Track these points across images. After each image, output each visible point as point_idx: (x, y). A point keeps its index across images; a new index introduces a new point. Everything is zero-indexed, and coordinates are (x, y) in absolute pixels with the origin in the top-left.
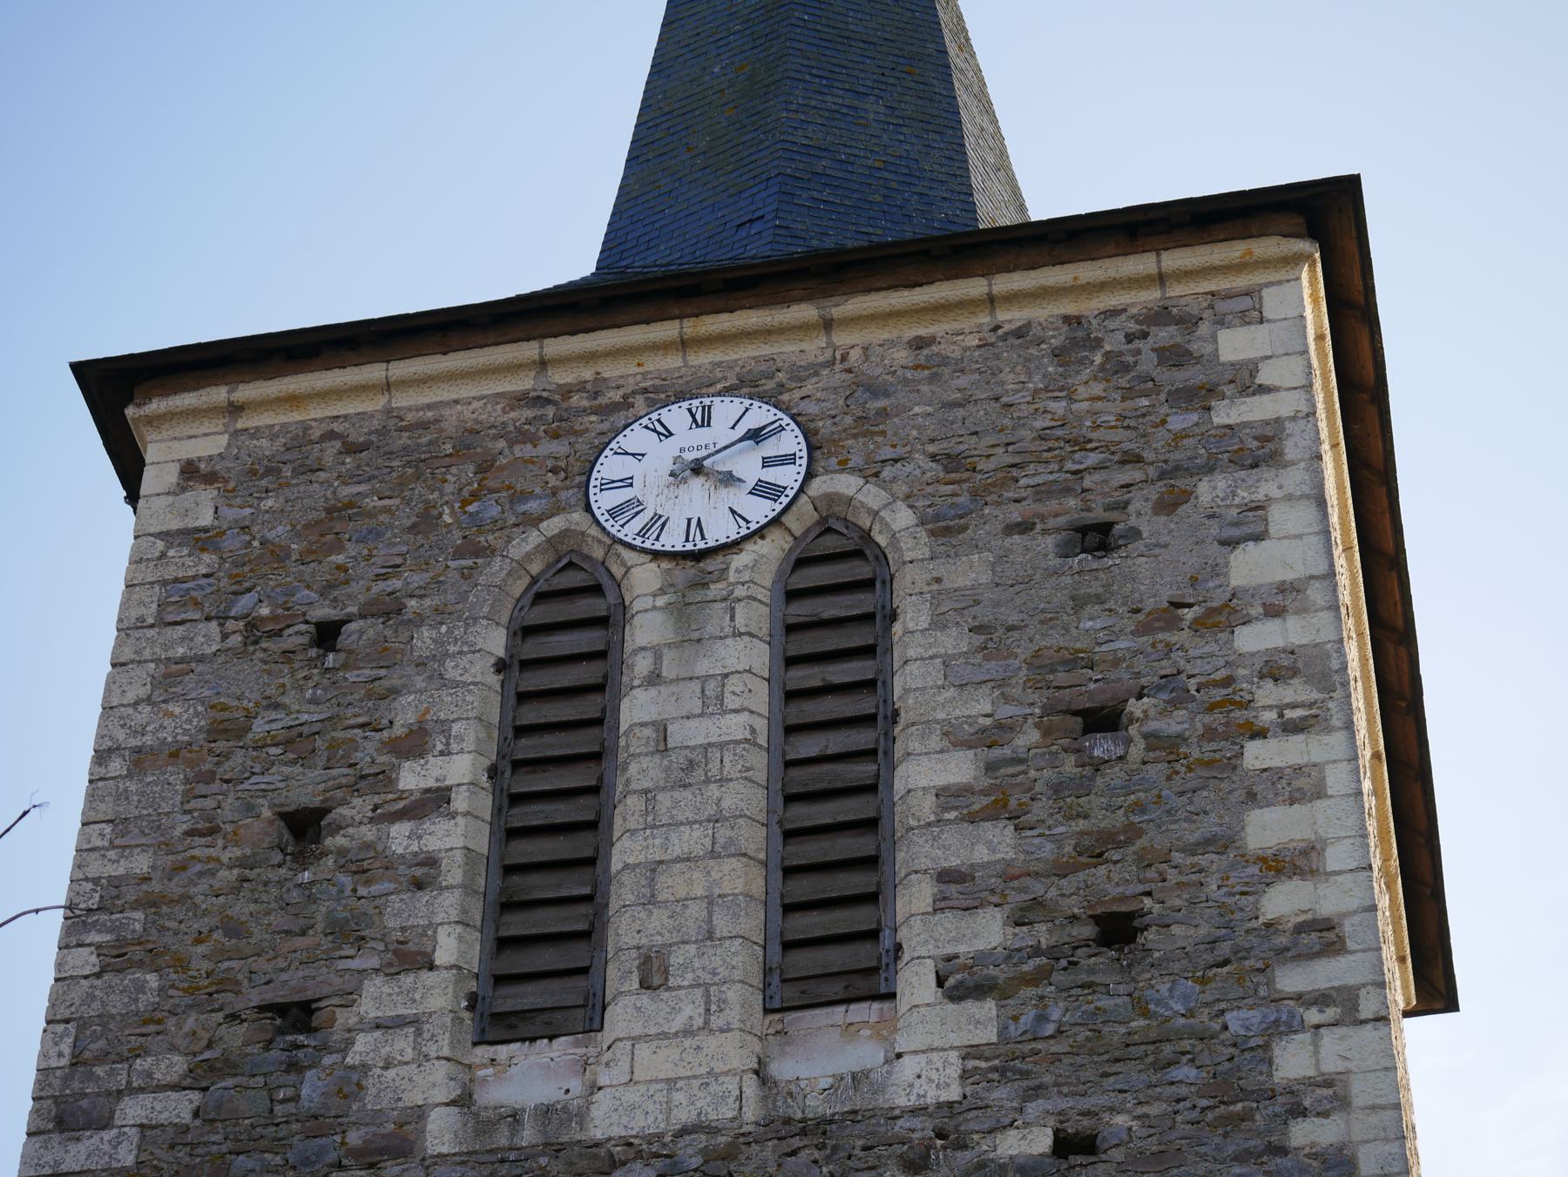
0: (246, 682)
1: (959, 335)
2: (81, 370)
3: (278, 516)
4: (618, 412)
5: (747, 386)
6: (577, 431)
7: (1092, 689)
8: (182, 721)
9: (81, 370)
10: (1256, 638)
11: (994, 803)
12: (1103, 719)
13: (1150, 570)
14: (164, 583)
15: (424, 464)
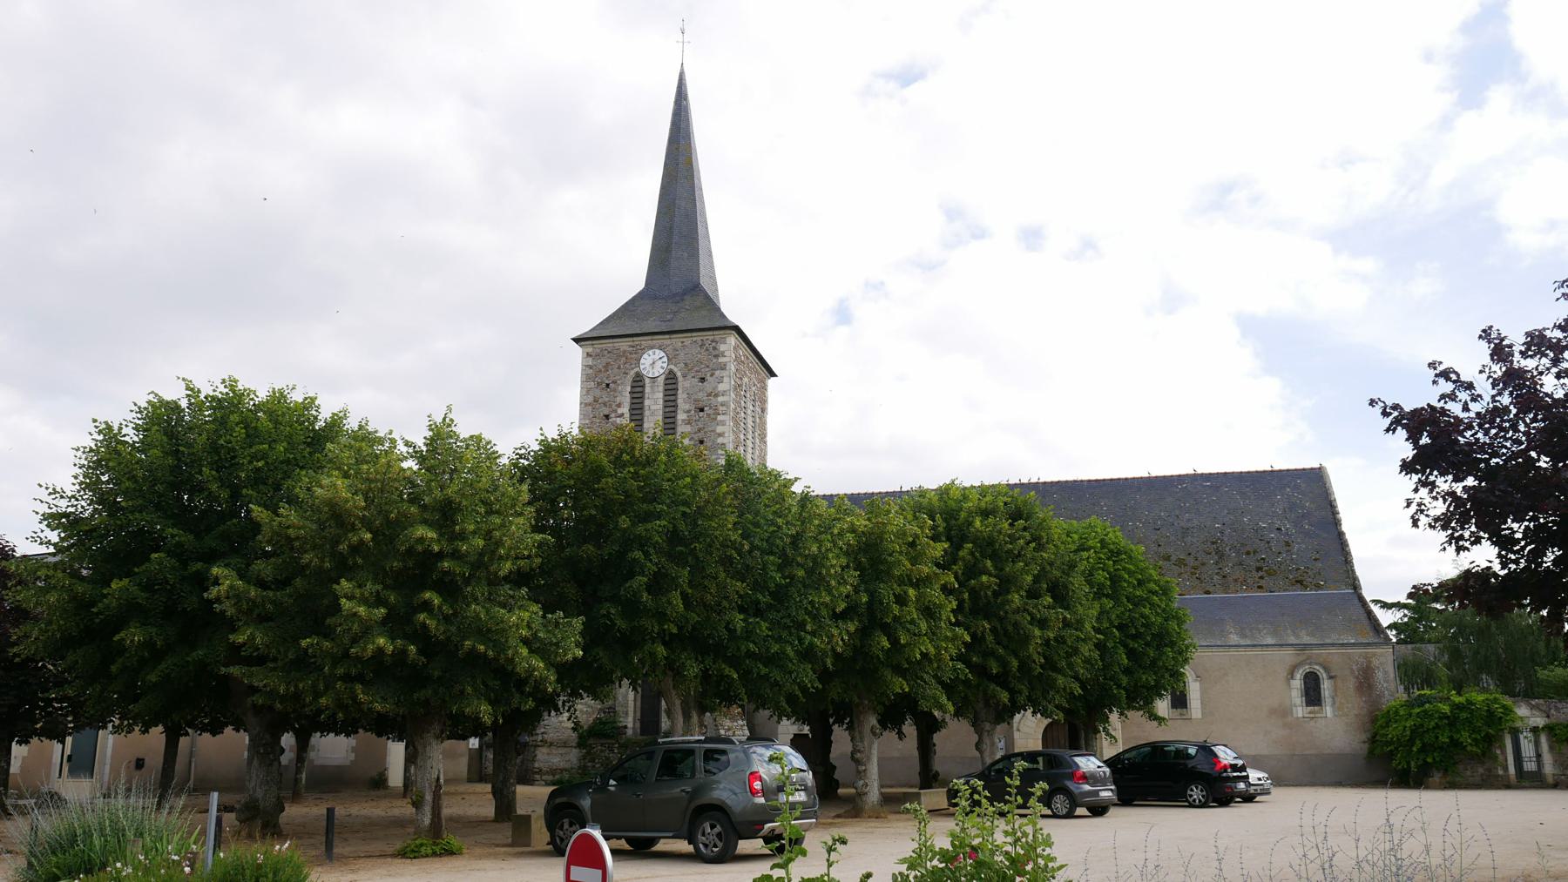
0: (598, 393)
1: (688, 342)
2: (1250, 326)
3: (600, 363)
4: (644, 350)
5: (660, 348)
6: (639, 353)
7: (701, 405)
8: (590, 399)
9: (1250, 326)
10: (720, 399)
11: (689, 423)
12: (702, 410)
13: (708, 386)
14: (129, 790)
15: (619, 356)
